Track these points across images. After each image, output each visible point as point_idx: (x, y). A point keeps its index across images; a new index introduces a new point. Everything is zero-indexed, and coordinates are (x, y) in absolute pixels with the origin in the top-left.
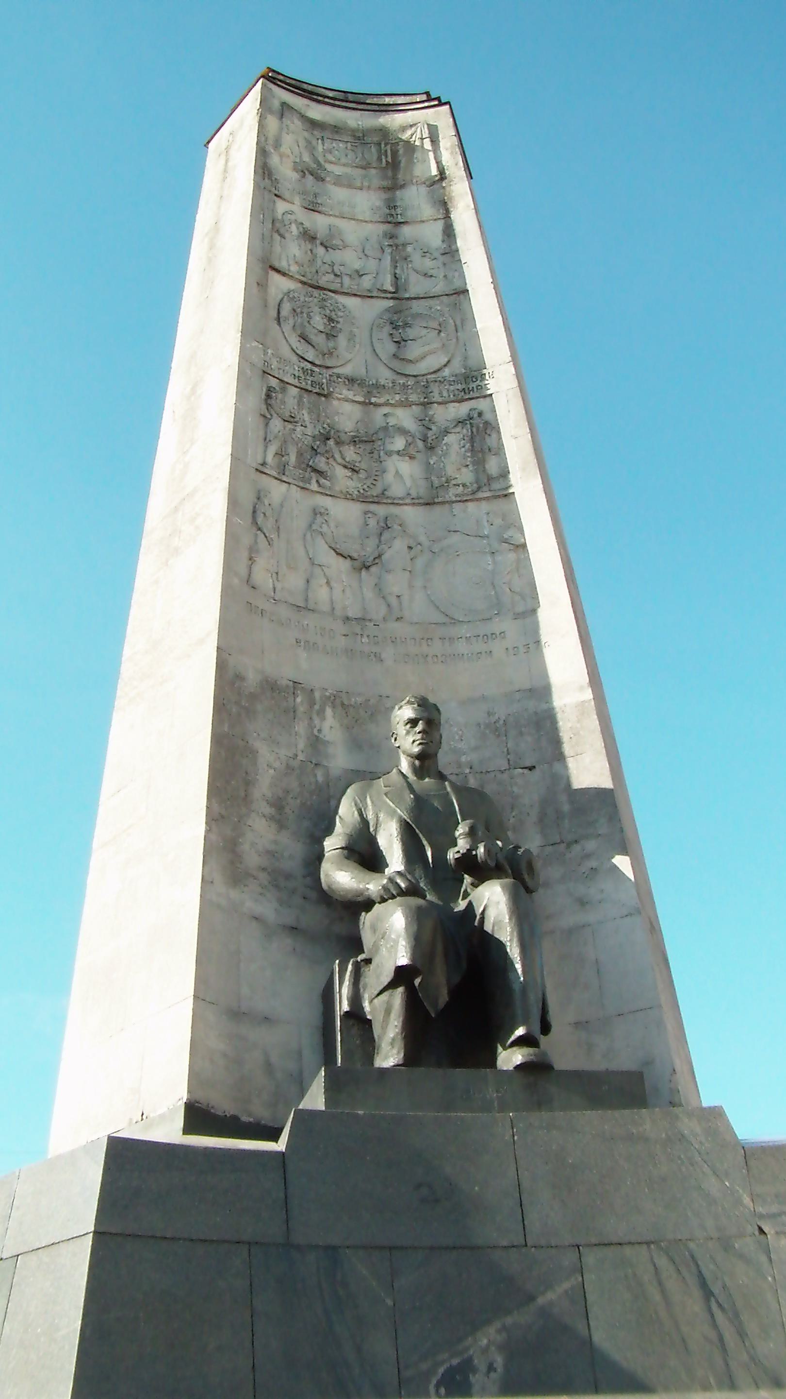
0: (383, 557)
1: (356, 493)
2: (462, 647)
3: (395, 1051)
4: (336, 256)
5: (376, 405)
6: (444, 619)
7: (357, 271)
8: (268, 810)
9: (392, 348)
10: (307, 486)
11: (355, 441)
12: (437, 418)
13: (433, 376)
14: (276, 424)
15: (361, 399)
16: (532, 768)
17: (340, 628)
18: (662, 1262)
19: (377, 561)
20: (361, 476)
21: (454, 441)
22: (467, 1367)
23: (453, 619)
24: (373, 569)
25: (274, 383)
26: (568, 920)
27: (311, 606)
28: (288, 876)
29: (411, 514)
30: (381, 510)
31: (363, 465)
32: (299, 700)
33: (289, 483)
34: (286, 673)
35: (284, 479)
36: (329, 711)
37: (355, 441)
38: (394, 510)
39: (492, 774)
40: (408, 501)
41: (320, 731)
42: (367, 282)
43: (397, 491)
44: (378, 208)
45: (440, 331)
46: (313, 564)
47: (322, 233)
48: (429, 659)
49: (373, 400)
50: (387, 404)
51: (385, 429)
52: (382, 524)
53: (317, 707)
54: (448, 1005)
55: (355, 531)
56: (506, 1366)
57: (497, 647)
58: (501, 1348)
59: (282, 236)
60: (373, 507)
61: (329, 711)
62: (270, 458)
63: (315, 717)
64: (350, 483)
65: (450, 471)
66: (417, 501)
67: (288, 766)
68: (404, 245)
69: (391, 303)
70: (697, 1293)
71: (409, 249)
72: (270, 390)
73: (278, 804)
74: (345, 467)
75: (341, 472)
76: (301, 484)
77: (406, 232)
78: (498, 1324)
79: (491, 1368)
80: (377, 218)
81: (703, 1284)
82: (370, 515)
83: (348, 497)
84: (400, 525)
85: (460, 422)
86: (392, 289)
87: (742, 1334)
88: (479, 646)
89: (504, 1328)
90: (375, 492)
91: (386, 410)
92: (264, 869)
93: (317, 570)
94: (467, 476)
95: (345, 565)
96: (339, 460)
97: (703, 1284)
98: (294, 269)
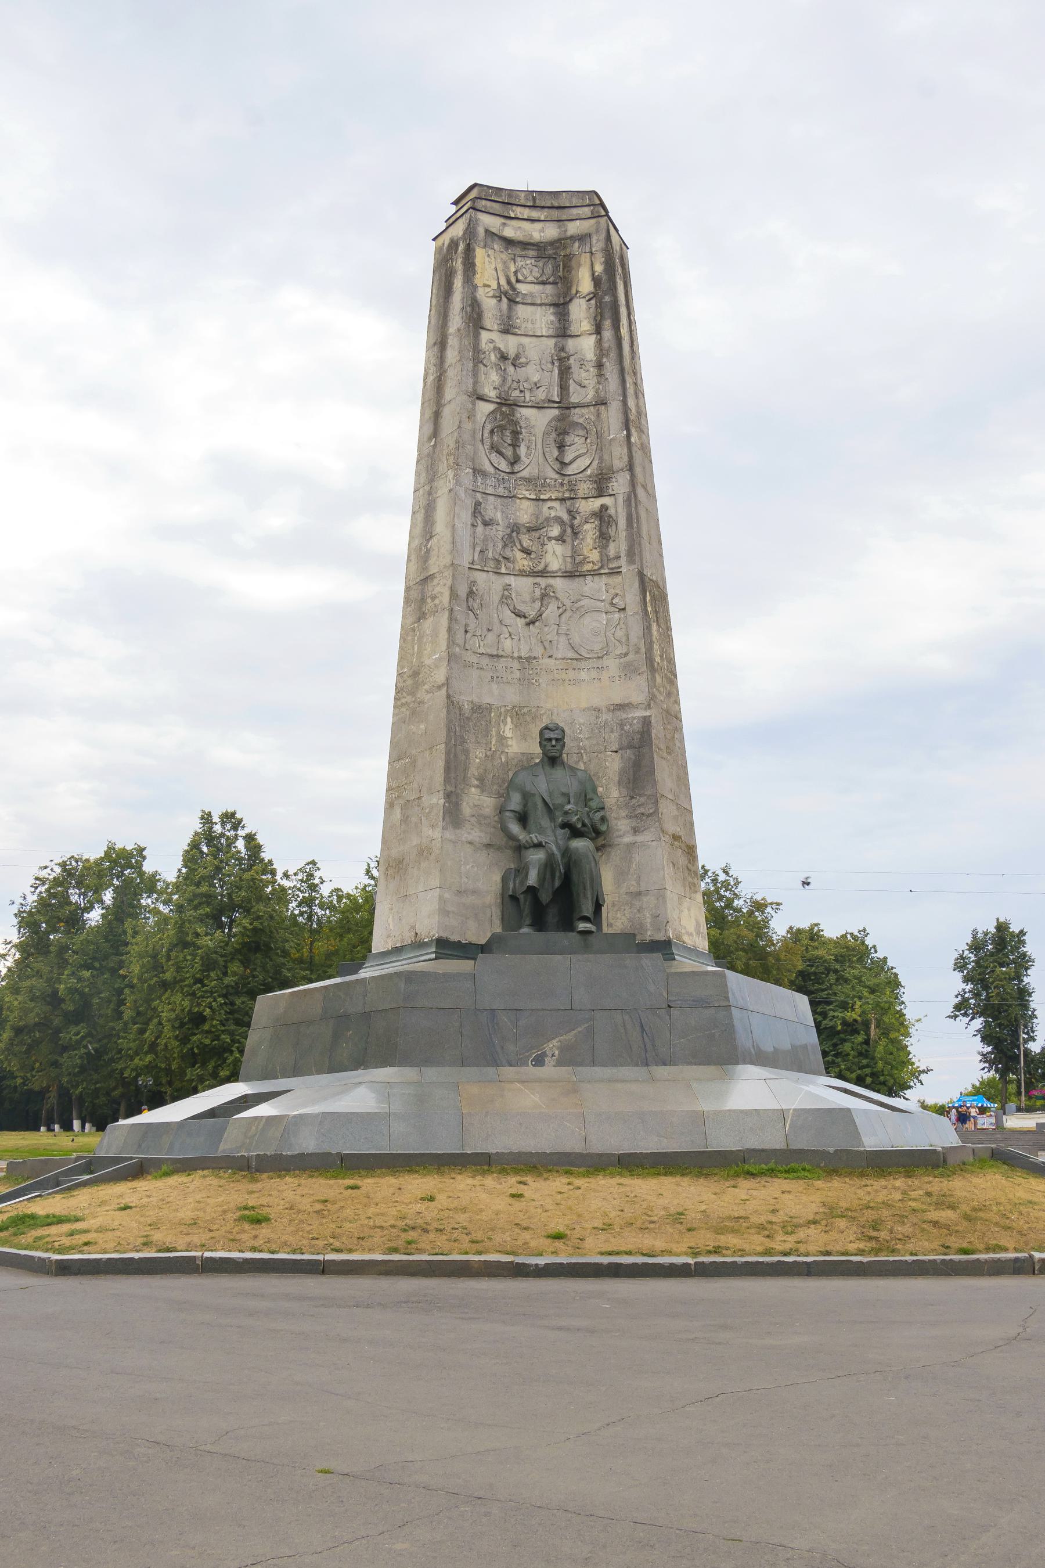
0: (544, 615)
1: (529, 569)
2: (583, 675)
3: (528, 919)
4: (522, 373)
5: (544, 500)
6: (575, 656)
7: (536, 384)
8: (476, 782)
9: (556, 453)
10: (498, 571)
11: (530, 530)
12: (581, 510)
13: (581, 475)
14: (480, 528)
15: (534, 497)
16: (616, 752)
17: (516, 665)
18: (626, 1017)
19: (539, 618)
20: (532, 556)
21: (590, 531)
22: (544, 1054)
23: (581, 655)
24: (537, 624)
25: (479, 496)
26: (628, 839)
27: (501, 653)
28: (485, 818)
29: (558, 583)
30: (543, 582)
31: (534, 549)
32: (492, 714)
33: (488, 571)
34: (487, 700)
35: (486, 569)
36: (509, 719)
37: (530, 530)
38: (551, 581)
39: (596, 754)
40: (559, 574)
41: (503, 732)
42: (541, 395)
43: (555, 565)
44: (552, 322)
45: (587, 438)
46: (502, 624)
47: (512, 353)
48: (566, 682)
49: (542, 497)
50: (550, 499)
51: (547, 519)
52: (543, 591)
53: (502, 718)
54: (558, 889)
55: (527, 597)
56: (559, 1054)
57: (605, 676)
58: (558, 1048)
59: (486, 366)
60: (538, 580)
61: (509, 719)
62: (476, 558)
63: (501, 724)
64: (526, 563)
65: (586, 551)
66: (565, 574)
67: (486, 756)
68: (568, 358)
69: (556, 412)
70: (638, 1028)
71: (572, 361)
72: (478, 504)
73: (481, 779)
74: (523, 552)
75: (519, 555)
76: (495, 570)
77: (570, 344)
78: (557, 1039)
79: (553, 1055)
80: (551, 332)
81: (642, 1026)
82: (536, 586)
83: (522, 573)
84: (554, 592)
85: (594, 514)
86: (558, 400)
87: (654, 1046)
88: (594, 674)
89: (560, 1041)
90: (540, 568)
91: (550, 504)
92: (473, 816)
93: (504, 629)
94: (595, 556)
95: (521, 622)
96: (519, 547)
97: (642, 1026)
98: (492, 394)
